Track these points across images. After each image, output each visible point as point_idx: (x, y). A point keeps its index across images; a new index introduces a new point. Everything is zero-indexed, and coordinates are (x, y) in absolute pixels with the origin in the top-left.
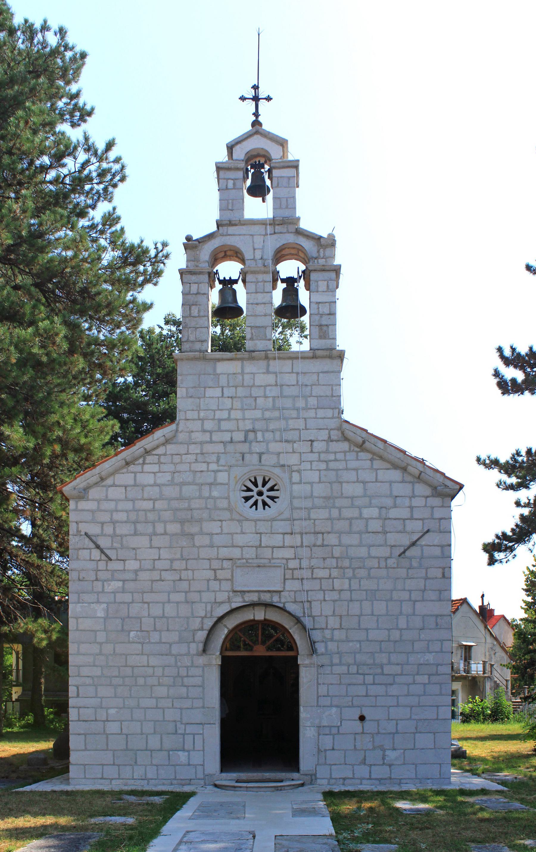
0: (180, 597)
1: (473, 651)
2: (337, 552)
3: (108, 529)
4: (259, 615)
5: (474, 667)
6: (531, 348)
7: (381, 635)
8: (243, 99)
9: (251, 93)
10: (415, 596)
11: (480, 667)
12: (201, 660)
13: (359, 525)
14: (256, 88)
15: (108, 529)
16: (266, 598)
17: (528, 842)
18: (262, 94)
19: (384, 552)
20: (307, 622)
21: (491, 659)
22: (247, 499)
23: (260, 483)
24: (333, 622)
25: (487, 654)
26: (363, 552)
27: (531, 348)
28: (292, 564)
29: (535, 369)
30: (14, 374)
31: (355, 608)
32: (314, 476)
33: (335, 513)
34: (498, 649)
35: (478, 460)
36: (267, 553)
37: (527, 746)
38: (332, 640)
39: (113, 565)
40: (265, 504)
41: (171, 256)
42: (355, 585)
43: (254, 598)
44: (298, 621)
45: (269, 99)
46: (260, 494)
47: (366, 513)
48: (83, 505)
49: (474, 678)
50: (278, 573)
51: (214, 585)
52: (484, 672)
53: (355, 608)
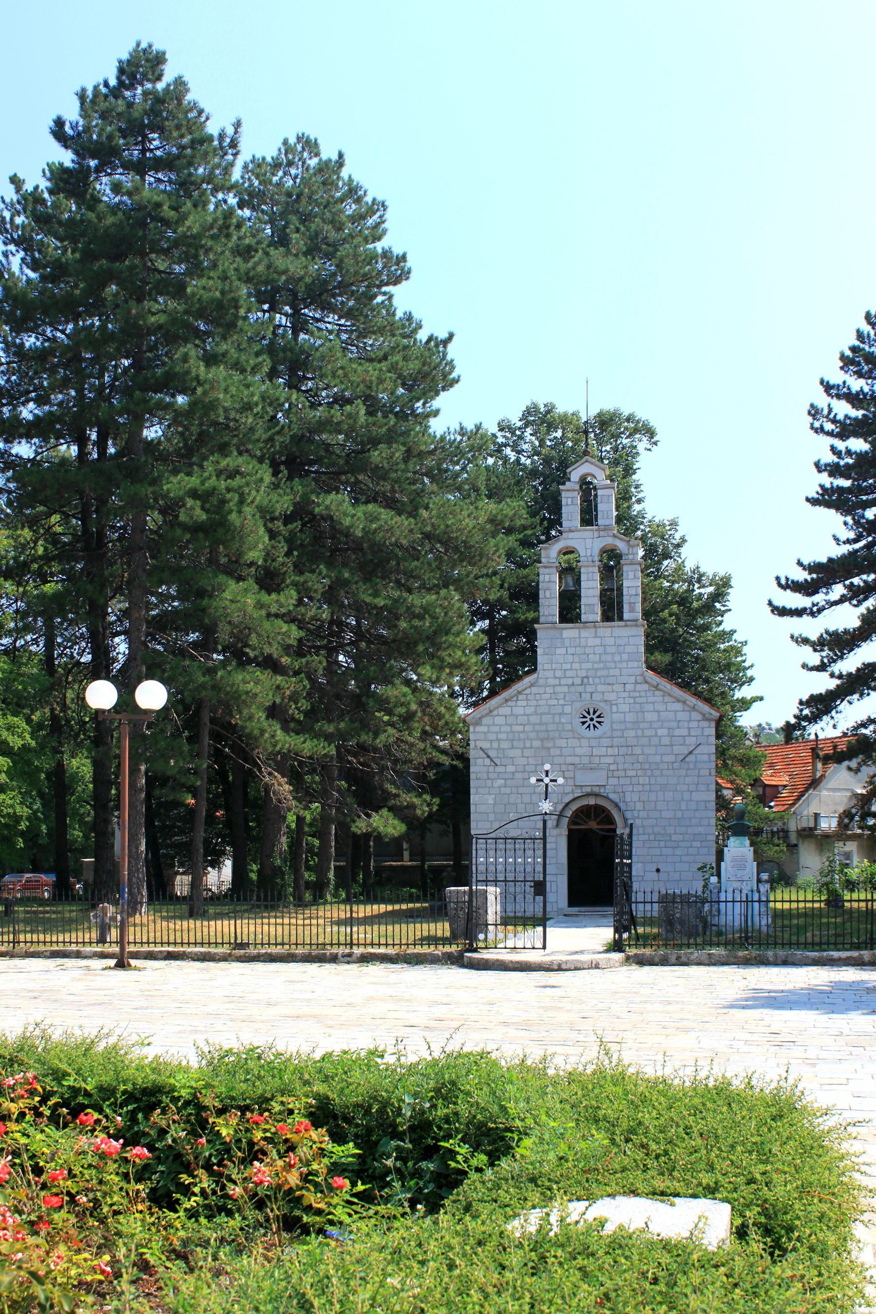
3: (495, 745)
22: (583, 723)
23: (591, 712)
28: (613, 767)
39: (498, 769)
40: (595, 726)
48: (479, 729)
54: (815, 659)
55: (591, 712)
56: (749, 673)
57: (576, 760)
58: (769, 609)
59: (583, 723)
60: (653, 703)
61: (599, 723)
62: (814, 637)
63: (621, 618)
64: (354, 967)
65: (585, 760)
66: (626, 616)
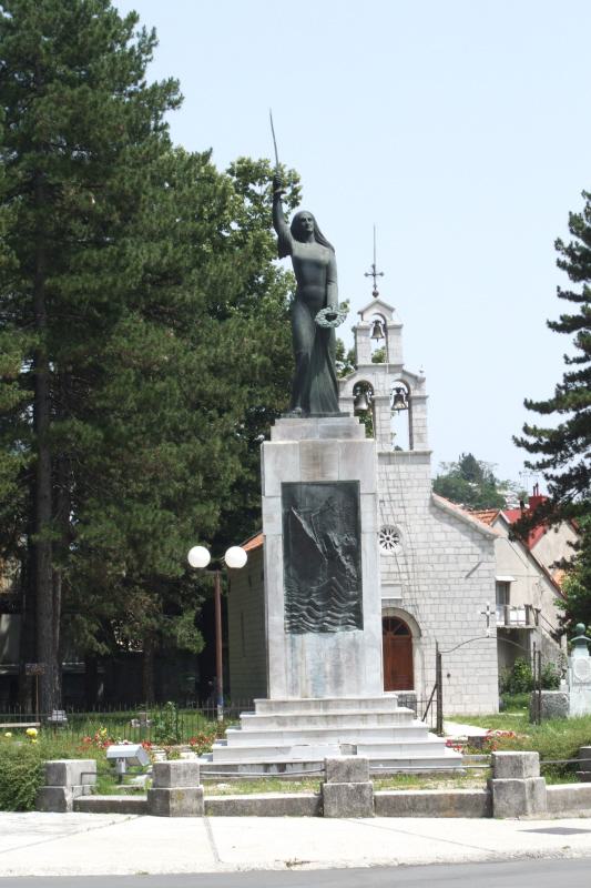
1: (513, 588)
2: (432, 575)
5: (513, 616)
6: (584, 194)
7: (458, 625)
8: (367, 275)
9: (370, 271)
10: (476, 601)
11: (522, 615)
13: (443, 559)
14: (374, 267)
17: (4, 672)
18: (378, 271)
19: (458, 574)
20: (418, 619)
21: (536, 602)
24: (431, 617)
25: (532, 593)
26: (446, 575)
27: (584, 194)
29: (590, 627)
31: (442, 609)
32: (418, 529)
33: (430, 551)
34: (545, 586)
37: (583, 367)
41: (184, 105)
44: (412, 617)
45: (382, 274)
47: (448, 551)
49: (514, 631)
52: (528, 623)
53: (442, 609)
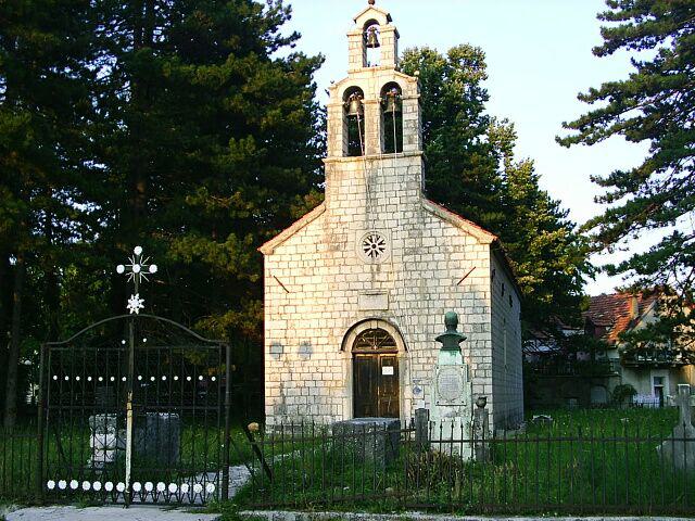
0: (328, 315)
3: (287, 272)
4: (374, 325)
12: (340, 356)
15: (287, 272)
16: (378, 314)
22: (366, 250)
23: (369, 242)
28: (393, 292)
30: (27, 362)
35: (599, 52)
36: (377, 285)
38: (418, 341)
39: (289, 296)
40: (381, 243)
42: (423, 320)
43: (370, 315)
46: (374, 246)
48: (272, 258)
50: (385, 298)
51: (347, 307)
54: (603, 191)
55: (369, 242)
56: (530, 160)
57: (360, 286)
58: (558, 144)
59: (366, 250)
60: (430, 229)
61: (381, 249)
62: (606, 177)
63: (400, 150)
64: (154, 511)
65: (368, 286)
66: (406, 147)
